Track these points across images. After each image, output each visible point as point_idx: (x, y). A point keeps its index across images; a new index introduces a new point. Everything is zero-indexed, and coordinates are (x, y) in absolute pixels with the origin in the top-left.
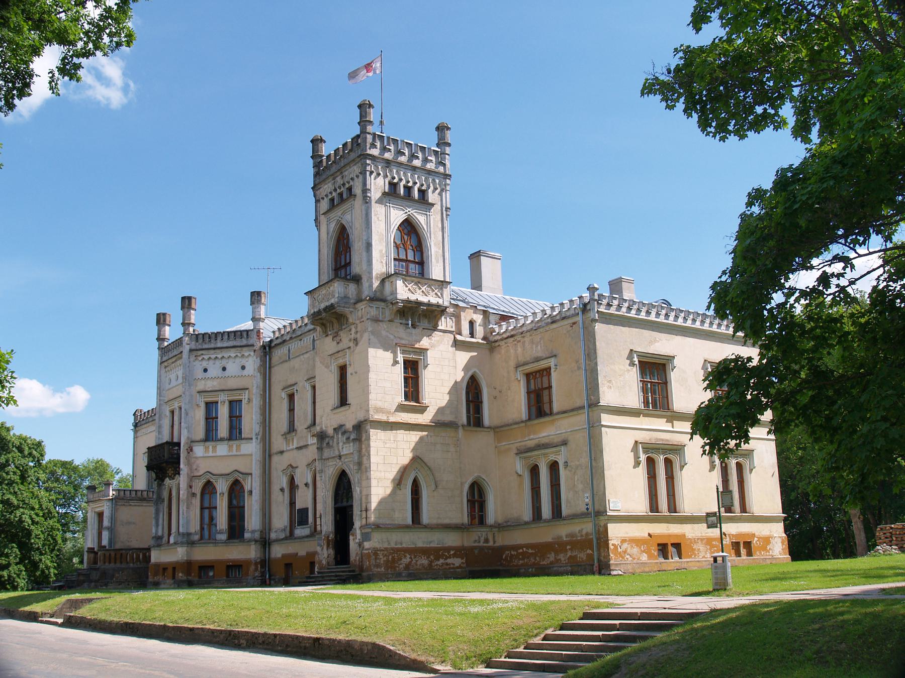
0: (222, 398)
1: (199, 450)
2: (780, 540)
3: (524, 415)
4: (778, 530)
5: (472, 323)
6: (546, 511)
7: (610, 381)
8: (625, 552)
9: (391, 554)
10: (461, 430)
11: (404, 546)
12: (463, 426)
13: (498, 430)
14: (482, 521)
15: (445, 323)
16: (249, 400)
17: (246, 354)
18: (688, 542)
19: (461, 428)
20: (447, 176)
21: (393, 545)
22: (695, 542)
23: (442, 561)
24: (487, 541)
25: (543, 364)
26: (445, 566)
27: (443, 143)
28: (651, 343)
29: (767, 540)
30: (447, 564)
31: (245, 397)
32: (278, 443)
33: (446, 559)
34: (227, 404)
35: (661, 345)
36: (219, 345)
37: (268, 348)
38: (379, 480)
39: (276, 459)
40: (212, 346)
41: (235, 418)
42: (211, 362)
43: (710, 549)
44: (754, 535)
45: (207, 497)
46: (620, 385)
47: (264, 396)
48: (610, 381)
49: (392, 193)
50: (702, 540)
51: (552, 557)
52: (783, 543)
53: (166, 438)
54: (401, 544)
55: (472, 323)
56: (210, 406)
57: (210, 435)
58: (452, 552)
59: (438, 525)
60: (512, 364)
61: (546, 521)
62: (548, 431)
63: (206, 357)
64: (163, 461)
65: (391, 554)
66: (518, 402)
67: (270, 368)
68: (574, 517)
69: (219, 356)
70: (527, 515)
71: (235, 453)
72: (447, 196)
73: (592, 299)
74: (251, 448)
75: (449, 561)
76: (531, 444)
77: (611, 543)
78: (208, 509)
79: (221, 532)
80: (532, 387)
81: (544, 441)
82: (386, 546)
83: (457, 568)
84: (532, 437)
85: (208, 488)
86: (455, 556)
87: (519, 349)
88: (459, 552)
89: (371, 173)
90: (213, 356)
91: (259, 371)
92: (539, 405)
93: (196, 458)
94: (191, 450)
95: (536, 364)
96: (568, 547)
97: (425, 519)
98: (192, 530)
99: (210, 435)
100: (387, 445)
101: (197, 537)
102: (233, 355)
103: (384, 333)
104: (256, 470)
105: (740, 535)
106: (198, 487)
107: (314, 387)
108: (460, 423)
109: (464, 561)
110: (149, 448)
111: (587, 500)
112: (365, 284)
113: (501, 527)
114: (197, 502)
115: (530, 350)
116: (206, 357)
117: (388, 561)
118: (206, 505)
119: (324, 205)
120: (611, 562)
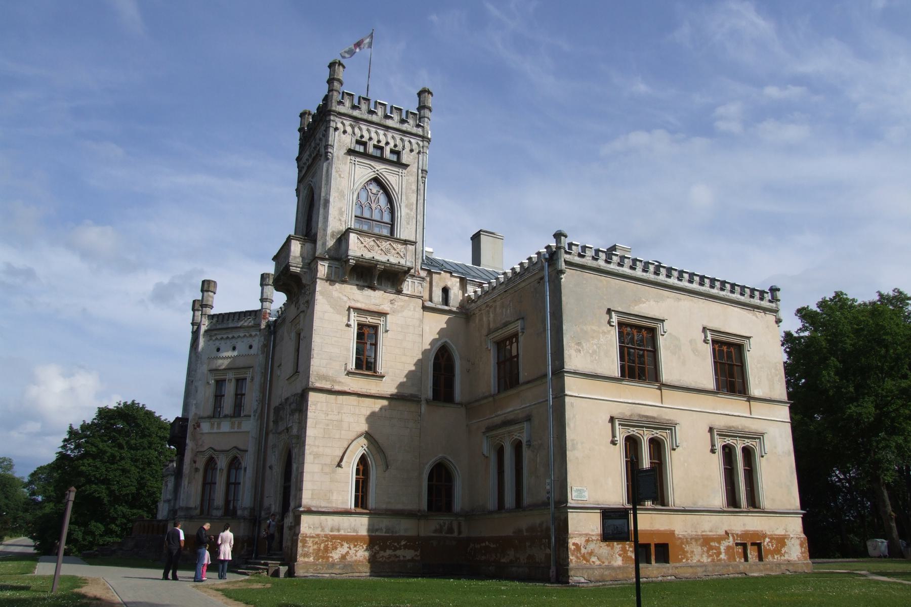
0: (231, 375)
1: (205, 427)
2: (798, 542)
3: (493, 388)
4: (794, 526)
5: (445, 291)
6: (509, 500)
7: (579, 344)
8: (591, 553)
9: (323, 541)
10: (424, 407)
11: (342, 533)
12: (427, 401)
13: (471, 407)
14: (448, 507)
15: (409, 286)
16: (252, 379)
17: (253, 333)
18: (678, 542)
19: (423, 402)
20: (424, 138)
21: (328, 532)
22: (687, 543)
23: (389, 552)
24: (450, 530)
25: (511, 329)
26: (392, 559)
27: (422, 107)
28: (638, 301)
29: (781, 541)
30: (396, 556)
31: (248, 376)
33: (395, 550)
34: (233, 381)
35: (649, 304)
36: (231, 325)
38: (317, 456)
40: (224, 326)
42: (223, 342)
43: (708, 552)
44: (764, 536)
45: (233, 472)
46: (590, 348)
47: (264, 375)
48: (579, 344)
49: (361, 151)
50: (696, 539)
51: (511, 554)
52: (801, 545)
54: (339, 530)
55: (445, 291)
56: (220, 383)
57: (216, 414)
58: (403, 543)
59: (387, 510)
60: (484, 331)
61: (510, 511)
62: (514, 406)
63: (219, 337)
65: (323, 541)
68: (534, 506)
69: (230, 336)
70: (492, 504)
71: (236, 430)
72: (425, 160)
73: (558, 248)
74: (249, 426)
75: (398, 553)
76: (498, 420)
77: (571, 541)
78: (208, 484)
79: (217, 509)
81: (511, 417)
82: (318, 532)
83: (409, 561)
84: (499, 413)
85: (211, 463)
86: (406, 547)
87: (491, 315)
88: (412, 542)
90: (225, 336)
91: (263, 353)
92: (509, 376)
93: (202, 434)
94: (199, 426)
95: (505, 330)
96: (528, 544)
98: (192, 505)
100: (330, 417)
101: (198, 511)
102: (242, 335)
103: (335, 294)
104: (251, 448)
105: (745, 534)
106: (201, 464)
108: (423, 397)
109: (418, 553)
111: (548, 487)
112: (319, 243)
113: (469, 515)
114: (199, 477)
116: (219, 337)
117: (319, 550)
118: (233, 480)
120: (571, 565)
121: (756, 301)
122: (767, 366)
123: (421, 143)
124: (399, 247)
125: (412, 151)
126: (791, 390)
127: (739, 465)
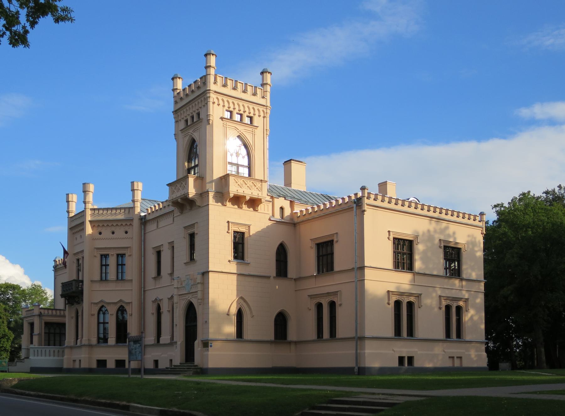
5: (282, 209)
15: (261, 207)
31: (127, 253)
32: (150, 283)
37: (144, 221)
39: (148, 293)
41: (120, 265)
53: (74, 277)
55: (282, 209)
57: (104, 279)
64: (71, 293)
66: (310, 261)
67: (145, 234)
80: (321, 254)
89: (214, 103)
97: (248, 334)
99: (104, 279)
106: (95, 310)
107: (173, 247)
110: (62, 284)
115: (320, 231)
119: (182, 125)
121: (471, 222)
122: (474, 268)
123: (265, 110)
124: (258, 185)
125: (259, 116)
126: (491, 345)
127: (453, 315)
